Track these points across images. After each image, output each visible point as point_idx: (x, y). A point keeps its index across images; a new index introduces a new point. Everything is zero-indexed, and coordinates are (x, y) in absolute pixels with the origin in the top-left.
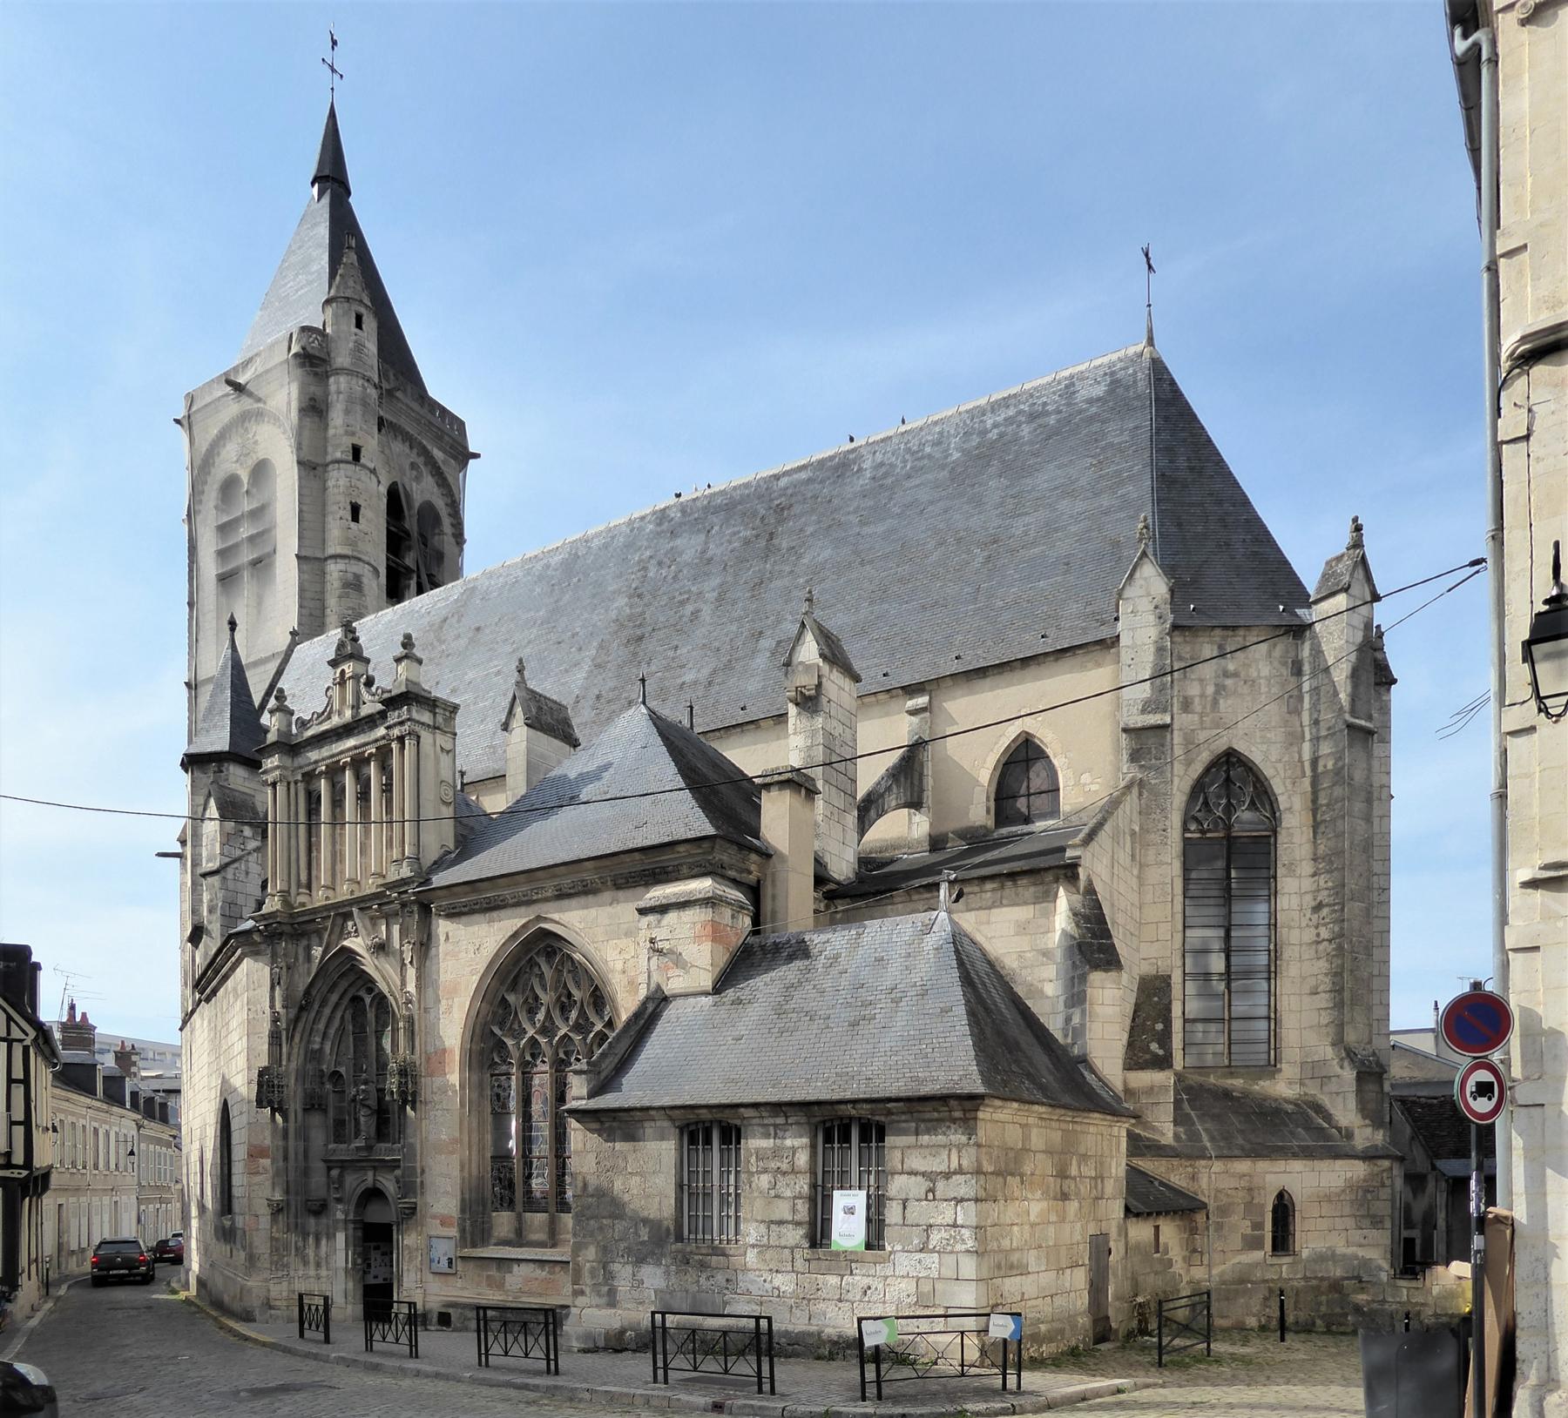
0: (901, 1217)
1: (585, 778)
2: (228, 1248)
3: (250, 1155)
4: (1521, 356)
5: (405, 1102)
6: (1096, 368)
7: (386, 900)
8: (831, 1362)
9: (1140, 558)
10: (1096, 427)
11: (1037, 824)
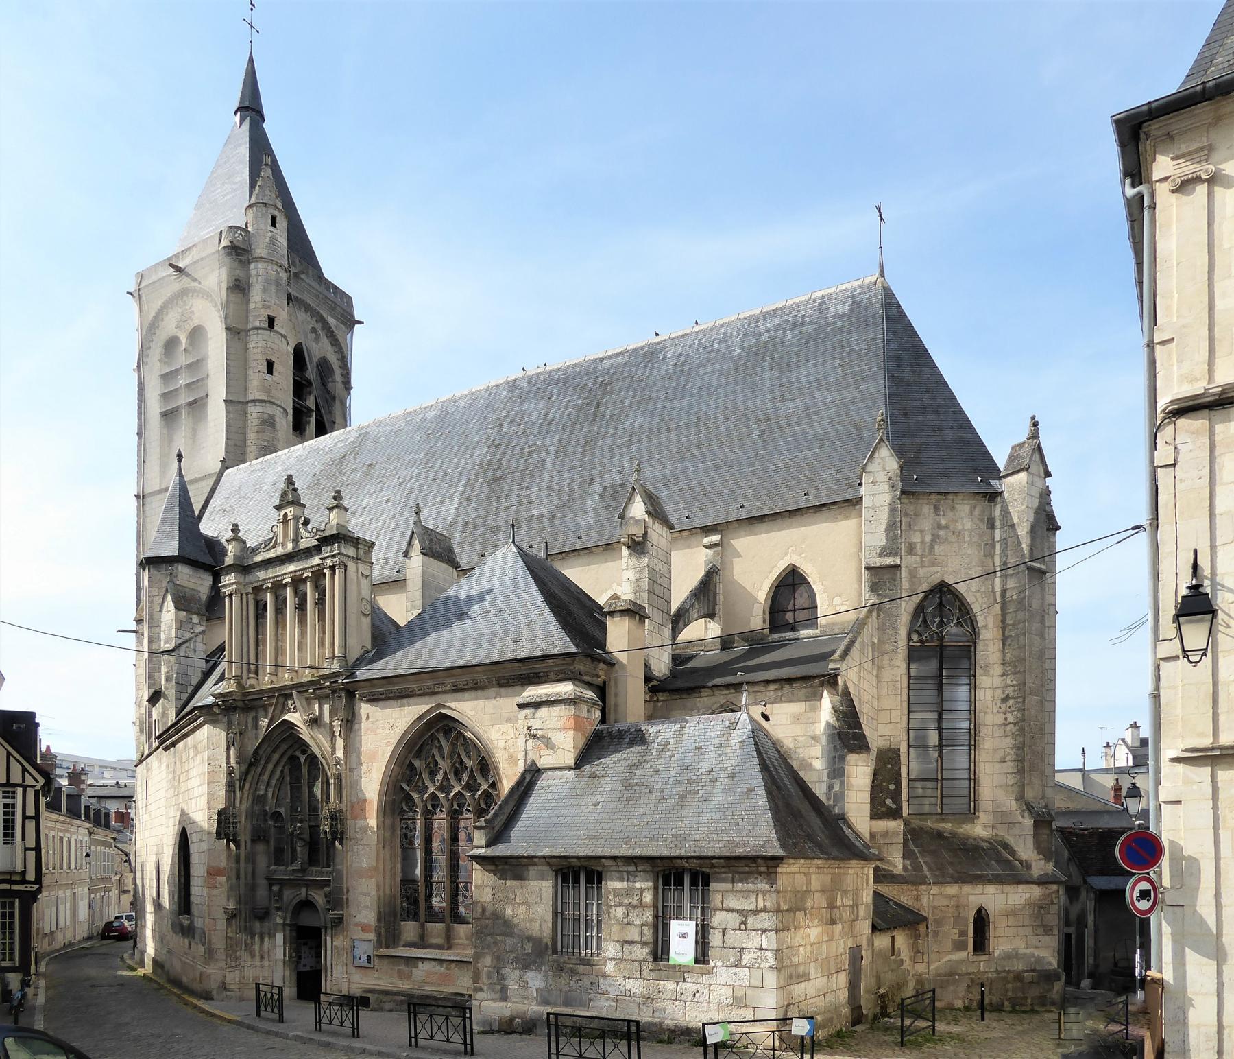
0: (721, 942)
1: (472, 600)
2: (186, 941)
3: (210, 874)
4: (1171, 412)
5: (334, 839)
6: (841, 291)
7: (318, 686)
8: (670, 1045)
9: (879, 443)
10: (842, 336)
11: (802, 632)
